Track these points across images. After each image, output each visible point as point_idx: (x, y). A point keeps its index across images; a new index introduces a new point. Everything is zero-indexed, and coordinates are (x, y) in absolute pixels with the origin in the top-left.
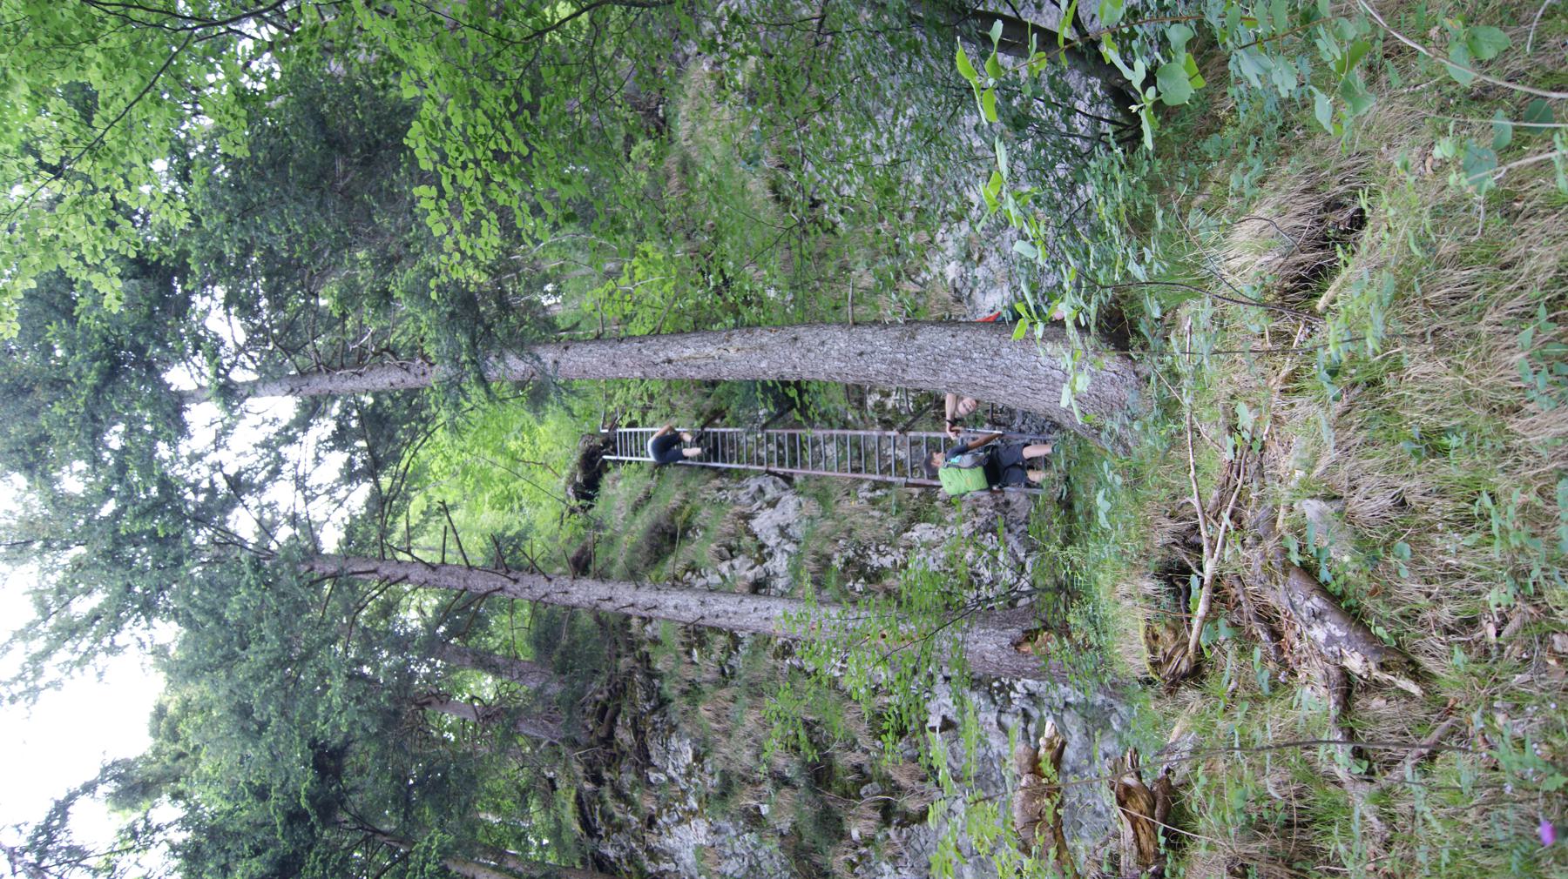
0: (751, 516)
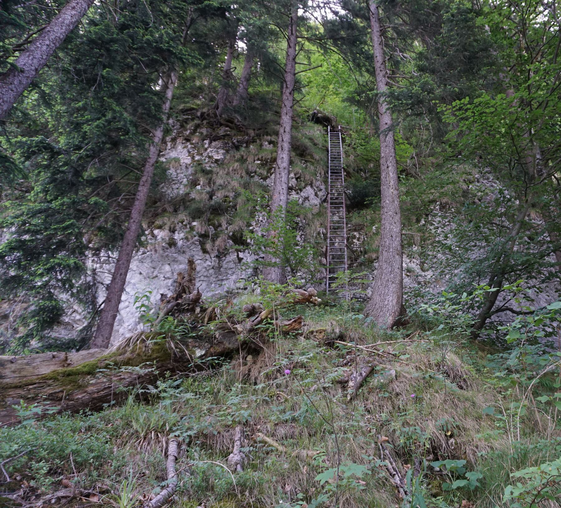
0: (312, 187)
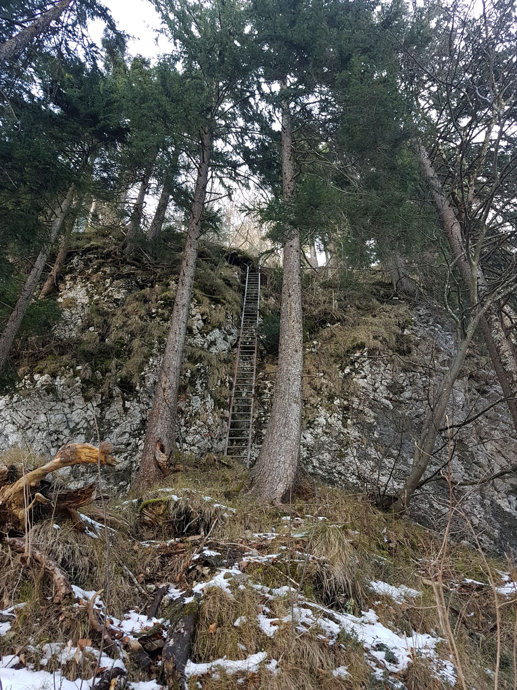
0: (220, 329)
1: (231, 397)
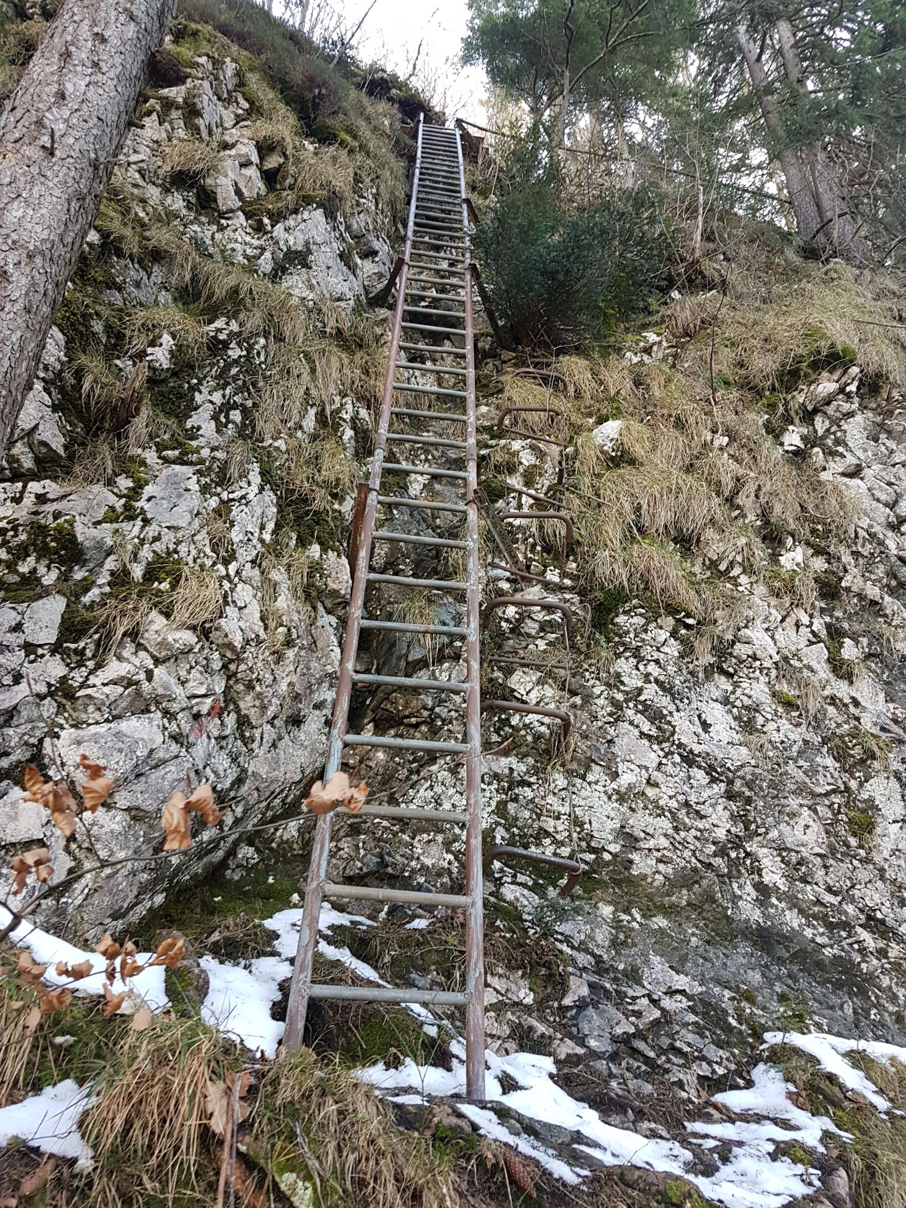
0: (330, 215)
1: (364, 489)
